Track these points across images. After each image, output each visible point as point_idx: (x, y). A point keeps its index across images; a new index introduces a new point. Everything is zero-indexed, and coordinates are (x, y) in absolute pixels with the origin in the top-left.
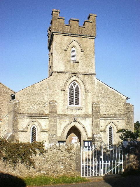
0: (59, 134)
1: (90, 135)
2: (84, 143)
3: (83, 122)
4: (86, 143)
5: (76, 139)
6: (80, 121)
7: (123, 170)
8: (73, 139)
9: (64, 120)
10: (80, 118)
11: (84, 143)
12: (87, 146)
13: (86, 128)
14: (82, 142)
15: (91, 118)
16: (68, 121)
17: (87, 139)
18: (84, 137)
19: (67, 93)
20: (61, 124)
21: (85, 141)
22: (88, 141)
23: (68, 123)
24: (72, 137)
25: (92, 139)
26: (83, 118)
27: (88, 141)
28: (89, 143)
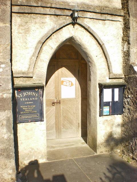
0: (21, 65)
1: (118, 69)
2: (101, 92)
3: (96, 27)
4: (107, 94)
5: (72, 84)
6: (87, 22)
7: (21, 107)
8: (65, 83)
9: (39, 18)
10: (89, 15)
11: (101, 92)
12: (111, 100)
13: (107, 47)
14: (94, 91)
15: (120, 19)
16: (50, 23)
17: (108, 81)
18: (100, 73)
19: (53, 78)
20: (27, 31)
21: (102, 87)
22: (112, 87)
23: (50, 27)
24: (62, 79)
25: (121, 81)
26: (98, 16)
27: (112, 87)
28: (117, 90)
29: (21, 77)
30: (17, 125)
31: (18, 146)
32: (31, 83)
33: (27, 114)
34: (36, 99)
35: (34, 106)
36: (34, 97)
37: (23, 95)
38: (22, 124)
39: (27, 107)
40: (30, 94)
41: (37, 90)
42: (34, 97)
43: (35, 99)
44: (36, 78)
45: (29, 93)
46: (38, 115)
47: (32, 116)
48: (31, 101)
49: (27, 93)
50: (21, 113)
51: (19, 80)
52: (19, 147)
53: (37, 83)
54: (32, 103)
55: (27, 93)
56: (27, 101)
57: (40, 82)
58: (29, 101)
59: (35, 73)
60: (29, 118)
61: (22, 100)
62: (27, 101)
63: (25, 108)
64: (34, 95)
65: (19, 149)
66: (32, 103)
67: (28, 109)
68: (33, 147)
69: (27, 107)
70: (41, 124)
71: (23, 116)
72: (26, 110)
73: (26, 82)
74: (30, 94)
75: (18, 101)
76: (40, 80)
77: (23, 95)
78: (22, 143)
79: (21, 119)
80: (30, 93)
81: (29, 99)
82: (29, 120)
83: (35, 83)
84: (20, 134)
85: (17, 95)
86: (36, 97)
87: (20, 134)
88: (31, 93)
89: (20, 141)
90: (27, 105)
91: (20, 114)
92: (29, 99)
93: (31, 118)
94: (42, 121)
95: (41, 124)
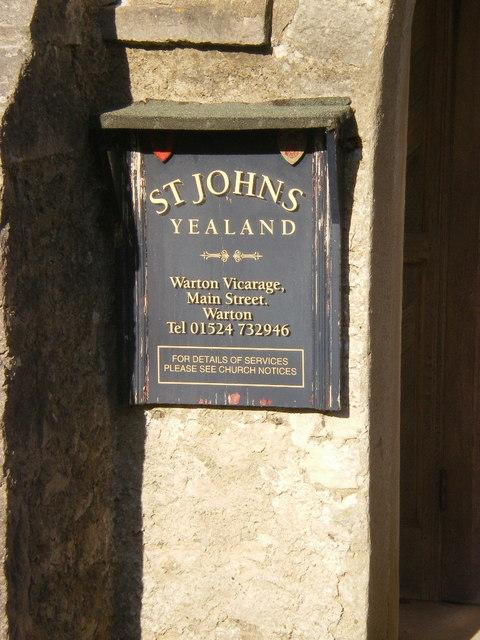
29: (170, 46)
30: (143, 419)
31: (144, 436)
32: (256, 98)
33: (215, 340)
34: (289, 228)
35: (271, 286)
36: (274, 212)
37: (187, 189)
38: (183, 418)
39: (213, 283)
40: (243, 188)
41: (291, 157)
42: (274, 212)
43: (278, 228)
44: (298, 54)
45: (239, 177)
46: (294, 360)
47: (250, 360)
48: (246, 243)
49: (217, 181)
50: (173, 328)
51: (166, 71)
52: (147, 599)
53: (304, 103)
54: (255, 256)
55: (217, 181)
56: (215, 243)
57: (328, 92)
58: (231, 244)
59: (292, 11)
60: (229, 377)
61: (184, 227)
62: (215, 243)
63: (202, 292)
64: (275, 197)
65: (145, 610)
66: (255, 256)
67: (222, 305)
68: (251, 620)
69: (213, 283)
70: (329, 437)
71: (185, 352)
72: (208, 312)
73: (222, 86)
74: (243, 188)
75: (150, 241)
76: (328, 76)
77: (187, 189)
78: (168, 569)
79: (166, 376)
80: (238, 181)
81: (236, 226)
82: (231, 391)
83: (286, 96)
84: (161, 497)
85: (147, 187)
86: (287, 216)
87: (161, 497)
88: (251, 183)
89: (158, 551)
90: (215, 269)
91: (167, 338)
92: (236, 226)
93: (240, 377)
94: (343, 411)
95: (323, 433)
